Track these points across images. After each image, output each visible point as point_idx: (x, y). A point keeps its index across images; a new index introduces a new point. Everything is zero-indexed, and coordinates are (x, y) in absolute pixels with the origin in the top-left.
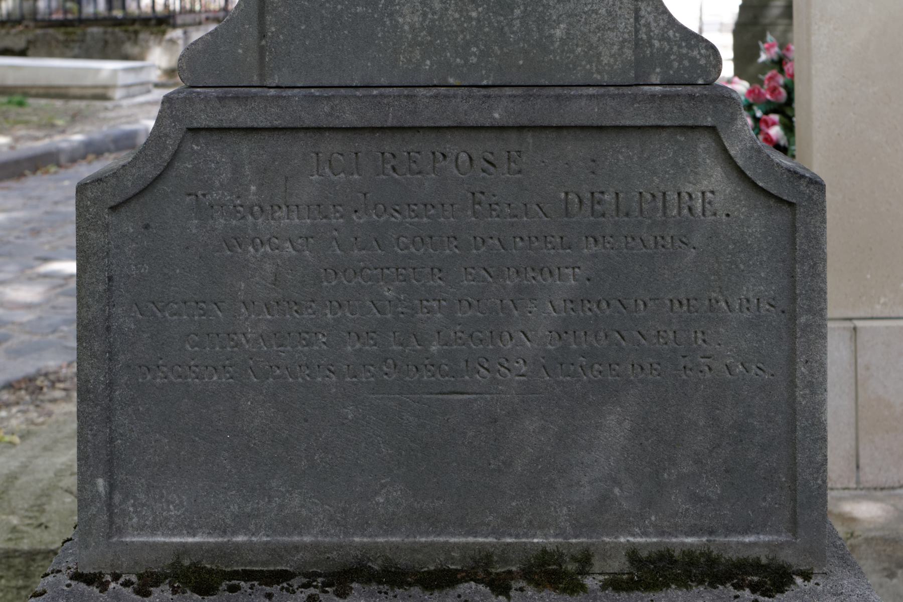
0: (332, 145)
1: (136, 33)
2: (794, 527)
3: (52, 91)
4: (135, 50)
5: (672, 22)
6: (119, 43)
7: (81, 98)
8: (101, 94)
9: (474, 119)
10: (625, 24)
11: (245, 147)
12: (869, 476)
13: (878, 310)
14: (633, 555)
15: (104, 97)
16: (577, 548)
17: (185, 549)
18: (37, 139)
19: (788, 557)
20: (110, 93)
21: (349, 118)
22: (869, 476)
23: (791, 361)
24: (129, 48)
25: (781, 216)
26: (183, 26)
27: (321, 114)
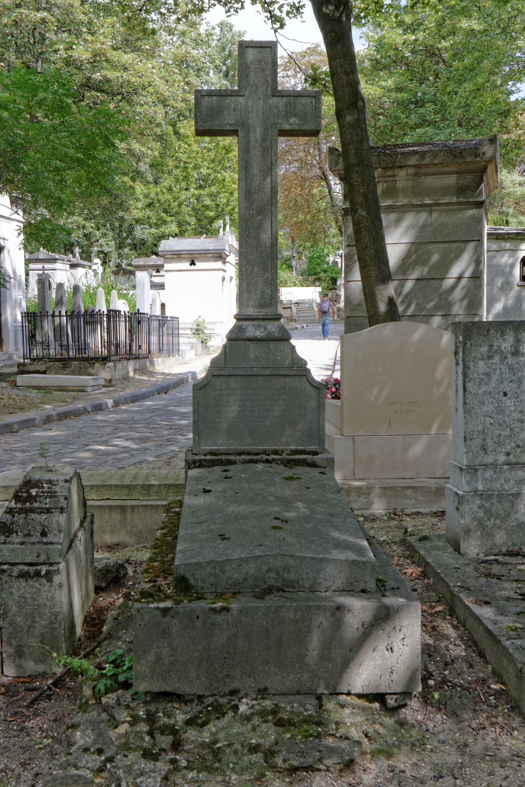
0: (239, 379)
1: (93, 364)
2: (319, 445)
3: (61, 388)
4: (93, 371)
5: (299, 356)
6: (86, 368)
7: (73, 391)
8: (82, 390)
9: (263, 373)
10: (290, 357)
11: (222, 379)
12: (357, 476)
13: (360, 434)
14: (291, 450)
15: (83, 391)
16: (288, 736)
17: (211, 450)
18: (63, 406)
19: (318, 450)
20: (86, 389)
21: (242, 373)
22: (357, 476)
23: (319, 416)
24: (90, 370)
25: (317, 391)
26: (113, 361)
27: (237, 373)
